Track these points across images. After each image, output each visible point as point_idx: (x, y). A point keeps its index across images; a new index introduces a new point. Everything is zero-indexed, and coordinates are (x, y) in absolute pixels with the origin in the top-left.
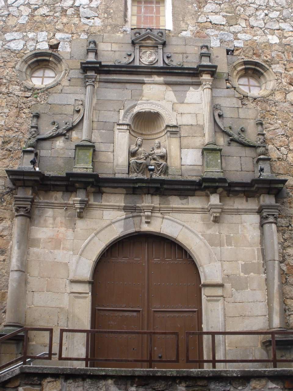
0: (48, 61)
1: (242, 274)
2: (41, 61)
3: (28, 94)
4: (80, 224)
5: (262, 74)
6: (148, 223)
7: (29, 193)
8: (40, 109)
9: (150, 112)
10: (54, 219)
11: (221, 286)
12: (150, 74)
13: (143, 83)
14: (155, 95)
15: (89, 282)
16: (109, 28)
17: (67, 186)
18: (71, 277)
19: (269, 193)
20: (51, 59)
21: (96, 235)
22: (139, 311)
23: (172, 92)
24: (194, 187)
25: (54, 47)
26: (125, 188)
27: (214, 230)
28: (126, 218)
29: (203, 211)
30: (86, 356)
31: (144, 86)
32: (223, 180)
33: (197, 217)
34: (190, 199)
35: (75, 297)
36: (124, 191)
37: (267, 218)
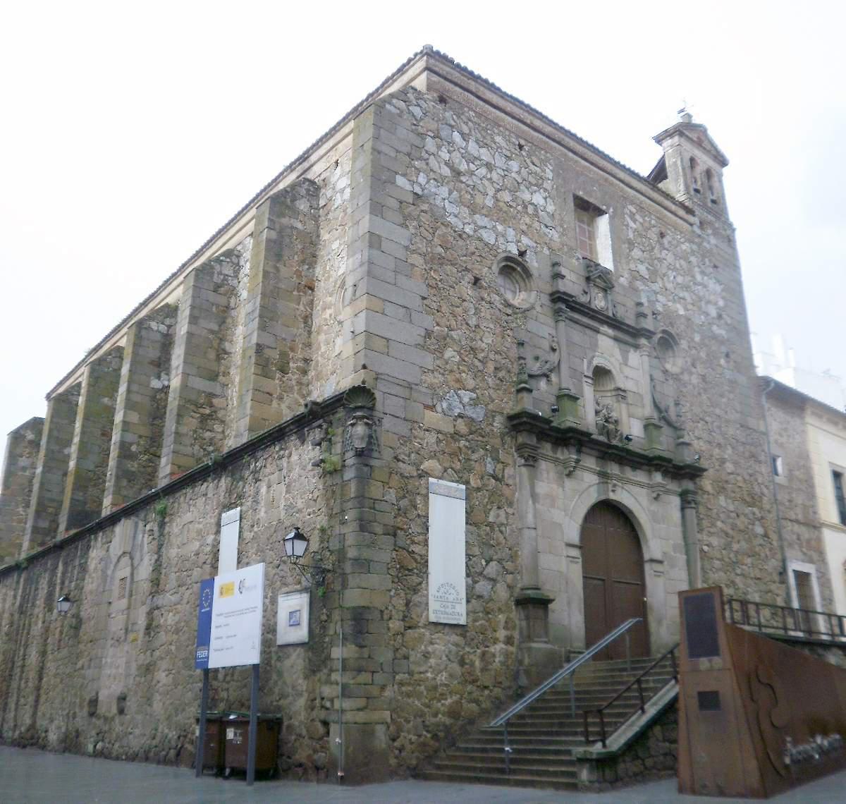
0: (514, 269)
1: (672, 553)
2: (514, 268)
3: (509, 311)
4: (568, 483)
5: (672, 347)
6: (613, 491)
7: (533, 440)
8: (523, 336)
9: (604, 368)
10: (548, 473)
11: (660, 562)
12: (602, 322)
13: (597, 331)
14: (606, 349)
15: (580, 548)
16: (566, 249)
17: (557, 439)
18: (566, 540)
19: (530, 432)
20: (519, 269)
21: (580, 495)
22: (603, 580)
23: (618, 350)
24: (642, 461)
25: (522, 254)
26: (598, 450)
27: (655, 507)
28: (599, 483)
29: (650, 487)
30: (263, 652)
31: (599, 335)
32: (669, 461)
33: (644, 491)
34: (639, 472)
35: (571, 561)
36: (596, 453)
37: (689, 503)
